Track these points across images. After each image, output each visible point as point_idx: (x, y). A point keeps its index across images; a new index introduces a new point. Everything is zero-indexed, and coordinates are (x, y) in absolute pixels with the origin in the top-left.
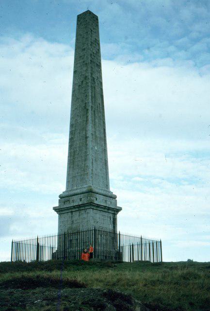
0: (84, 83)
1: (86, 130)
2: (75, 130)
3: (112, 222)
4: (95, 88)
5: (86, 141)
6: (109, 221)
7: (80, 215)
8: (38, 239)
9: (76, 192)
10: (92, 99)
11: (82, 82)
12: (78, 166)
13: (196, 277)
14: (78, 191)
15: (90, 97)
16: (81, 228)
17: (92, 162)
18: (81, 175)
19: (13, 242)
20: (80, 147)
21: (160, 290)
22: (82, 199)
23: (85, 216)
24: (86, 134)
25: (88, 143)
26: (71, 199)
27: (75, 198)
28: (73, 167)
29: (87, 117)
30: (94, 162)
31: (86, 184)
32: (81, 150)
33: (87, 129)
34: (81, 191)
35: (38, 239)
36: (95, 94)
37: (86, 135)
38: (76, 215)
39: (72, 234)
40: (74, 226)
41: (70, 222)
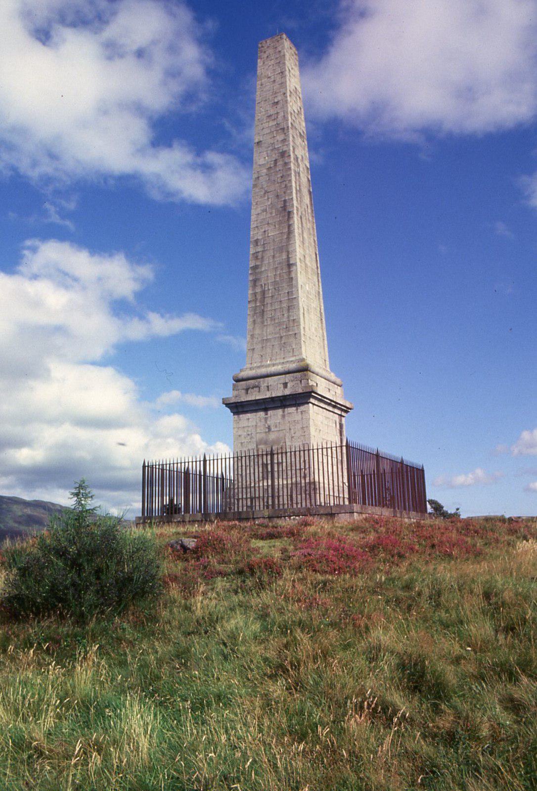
0: (280, 163)
1: (288, 252)
2: (263, 251)
3: (338, 431)
4: (299, 173)
5: (290, 272)
6: (335, 430)
7: (283, 416)
8: (205, 461)
9: (273, 369)
10: (296, 194)
11: (276, 160)
12: (273, 319)
13: (39, 522)
14: (279, 368)
15: (294, 191)
16: (288, 444)
17: (304, 314)
18: (281, 337)
19: (144, 467)
20: (275, 283)
21: (423, 580)
22: (289, 385)
23: (298, 417)
24: (288, 258)
25: (293, 275)
26: (264, 383)
27: (270, 380)
28: (263, 322)
29: (289, 226)
30: (305, 313)
31: (293, 356)
32: (277, 290)
33: (290, 249)
34: (286, 369)
35: (205, 461)
36: (300, 186)
37: (288, 261)
38: (276, 416)
39: (262, 455)
40: (272, 436)
41: (261, 429)
